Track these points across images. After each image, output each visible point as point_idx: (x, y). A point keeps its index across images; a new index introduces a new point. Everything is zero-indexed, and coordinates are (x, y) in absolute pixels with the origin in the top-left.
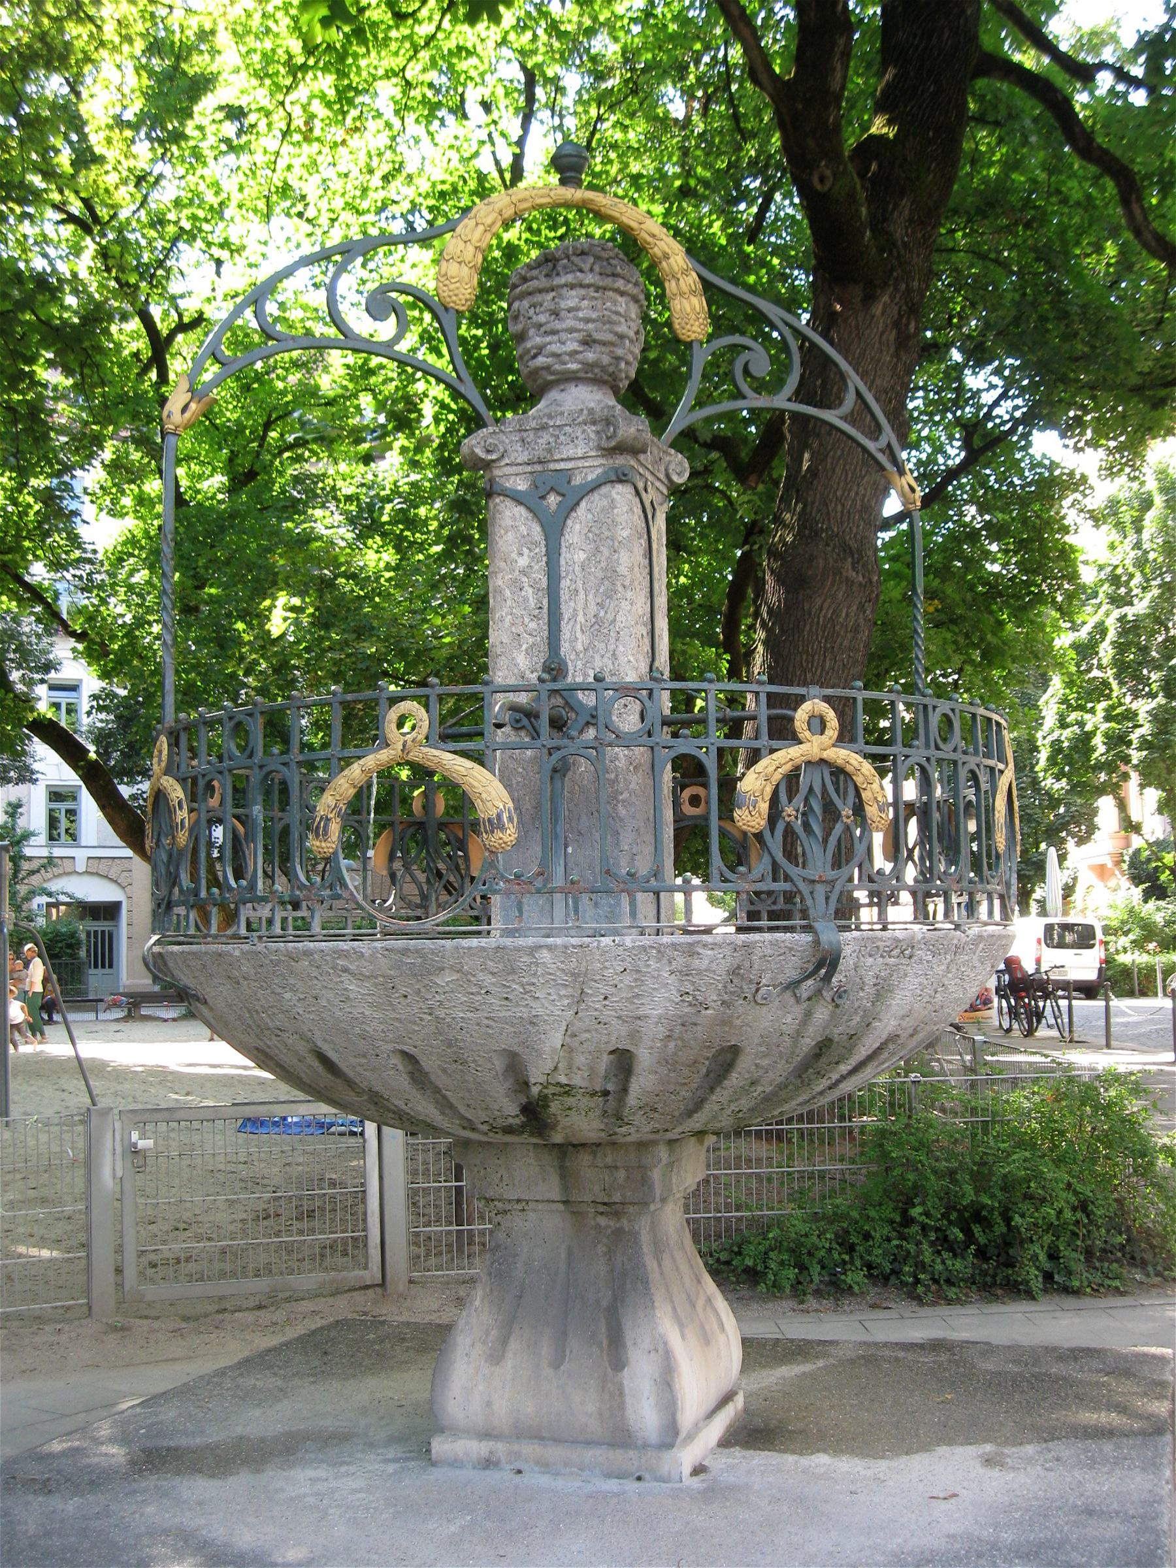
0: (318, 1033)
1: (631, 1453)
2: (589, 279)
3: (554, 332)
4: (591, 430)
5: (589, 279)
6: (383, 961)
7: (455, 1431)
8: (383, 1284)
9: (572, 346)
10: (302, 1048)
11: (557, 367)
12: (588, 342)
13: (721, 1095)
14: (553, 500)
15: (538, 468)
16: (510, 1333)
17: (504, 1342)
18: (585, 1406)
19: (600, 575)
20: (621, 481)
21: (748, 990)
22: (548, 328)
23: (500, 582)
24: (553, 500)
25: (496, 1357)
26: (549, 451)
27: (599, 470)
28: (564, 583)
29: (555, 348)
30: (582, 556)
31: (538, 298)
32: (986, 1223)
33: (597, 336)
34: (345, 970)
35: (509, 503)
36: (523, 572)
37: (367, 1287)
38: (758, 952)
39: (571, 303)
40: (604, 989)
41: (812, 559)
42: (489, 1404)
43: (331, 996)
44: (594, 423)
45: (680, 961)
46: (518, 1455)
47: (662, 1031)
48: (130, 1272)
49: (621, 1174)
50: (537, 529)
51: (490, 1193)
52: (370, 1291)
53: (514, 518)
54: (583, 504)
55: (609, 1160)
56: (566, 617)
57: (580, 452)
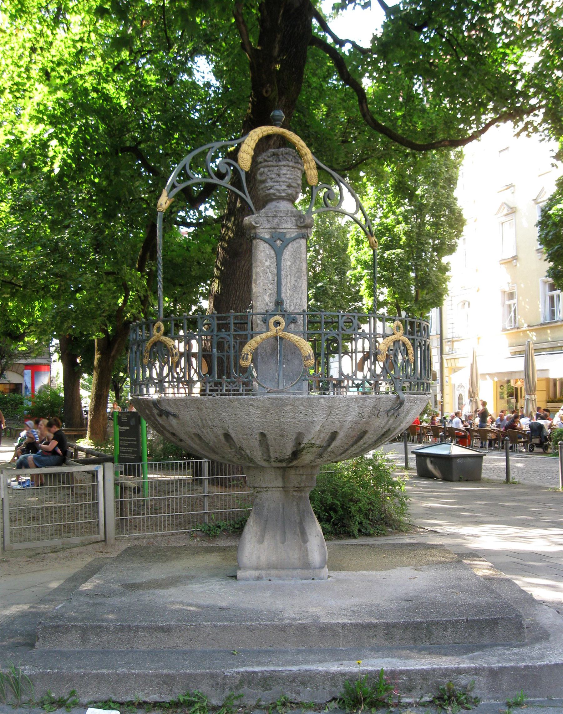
0: (231, 427)
1: (310, 571)
2: (291, 164)
3: (277, 182)
4: (293, 219)
5: (291, 164)
6: (267, 402)
7: (246, 568)
8: (105, 541)
9: (284, 187)
10: (220, 432)
11: (278, 194)
12: (289, 186)
13: (355, 447)
14: (279, 242)
15: (274, 230)
16: (265, 533)
17: (263, 536)
18: (294, 556)
19: (296, 270)
20: (303, 238)
21: (377, 412)
22: (276, 180)
23: (258, 270)
24: (279, 242)
25: (261, 541)
26: (278, 225)
27: (296, 234)
28: (283, 272)
29: (278, 187)
30: (289, 263)
31: (272, 168)
32: (335, 511)
33: (293, 185)
34: (252, 405)
35: (262, 242)
36: (268, 267)
37: (98, 542)
38: (382, 400)
39: (284, 172)
40: (338, 412)
41: (241, 245)
42: (259, 558)
43: (242, 414)
44: (294, 216)
45: (361, 402)
46: (269, 575)
47: (349, 425)
48: (7, 538)
49: (304, 477)
50: (272, 252)
51: (256, 485)
52: (100, 544)
53: (264, 248)
54: (290, 245)
55: (301, 472)
56: (283, 284)
57: (289, 226)
